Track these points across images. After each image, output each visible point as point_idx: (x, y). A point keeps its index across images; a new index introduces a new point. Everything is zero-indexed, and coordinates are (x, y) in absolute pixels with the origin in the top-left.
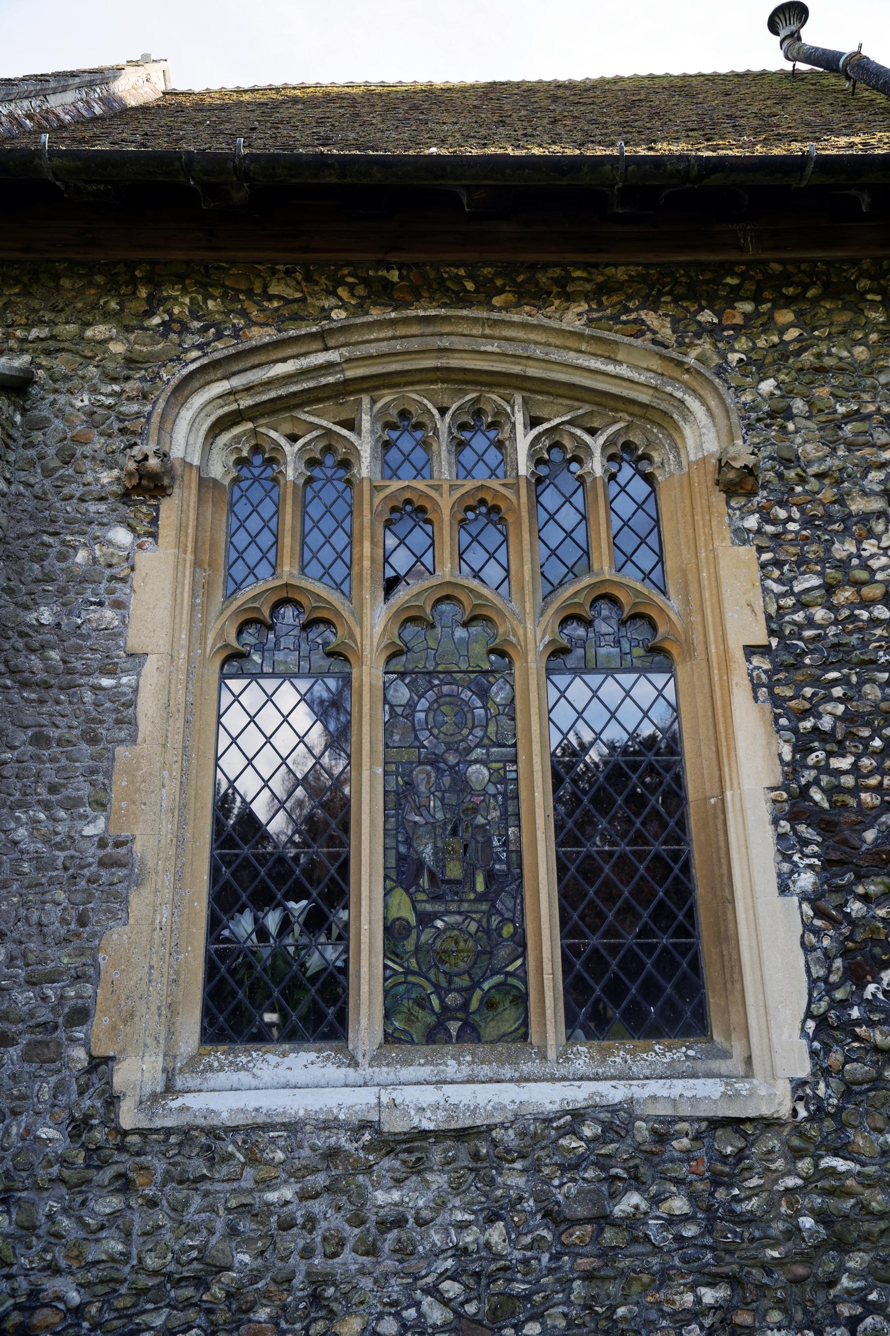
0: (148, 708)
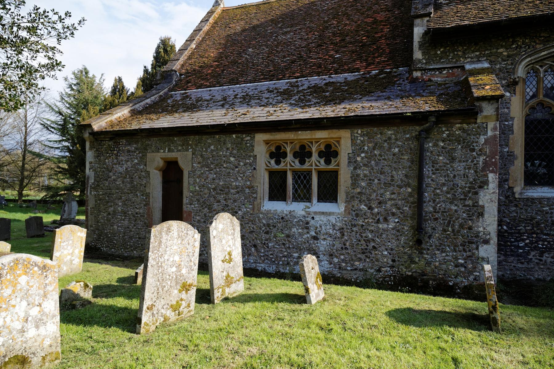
0: (515, 127)
